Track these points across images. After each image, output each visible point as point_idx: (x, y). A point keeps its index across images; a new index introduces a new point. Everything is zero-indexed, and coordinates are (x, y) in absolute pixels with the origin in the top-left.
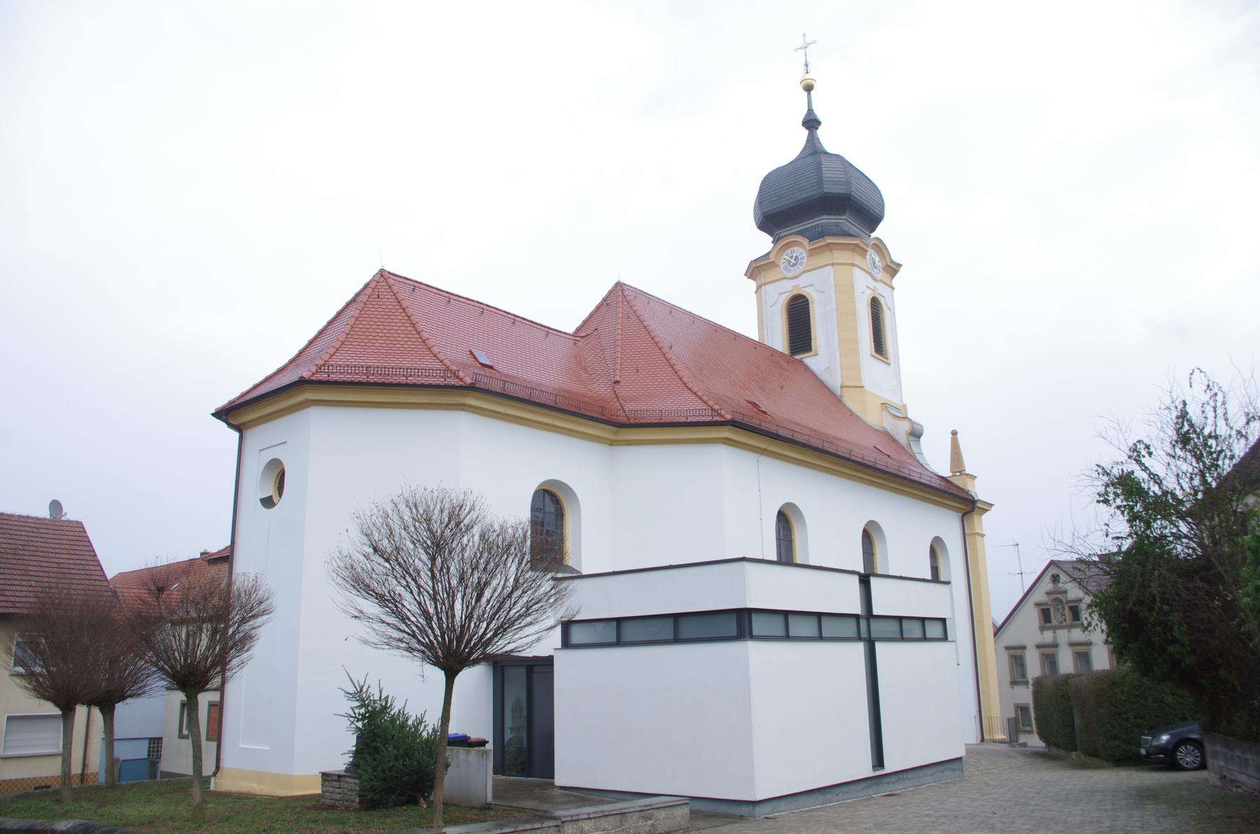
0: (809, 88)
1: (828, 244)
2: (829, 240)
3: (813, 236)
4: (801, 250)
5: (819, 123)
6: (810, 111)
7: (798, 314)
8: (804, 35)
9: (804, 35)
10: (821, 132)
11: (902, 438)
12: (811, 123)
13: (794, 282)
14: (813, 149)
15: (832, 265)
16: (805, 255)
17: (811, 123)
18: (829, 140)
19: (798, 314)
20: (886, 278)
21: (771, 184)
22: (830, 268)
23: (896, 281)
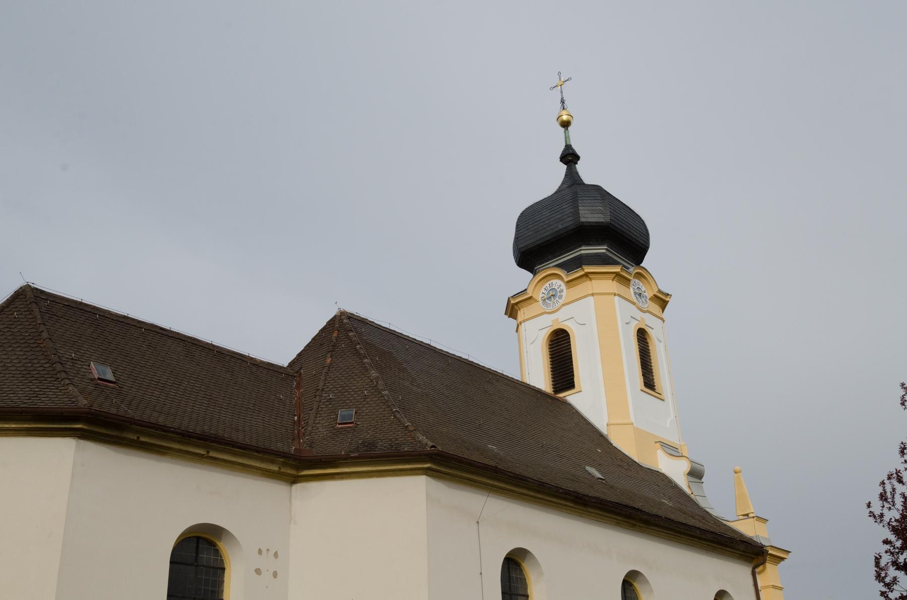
0: (566, 125)
1: (586, 275)
2: (588, 269)
3: (568, 267)
5: (578, 158)
6: (568, 147)
7: (560, 347)
8: (559, 74)
9: (559, 74)
10: (580, 167)
11: (682, 481)
12: (570, 157)
14: (572, 179)
15: (593, 295)
16: (563, 287)
17: (570, 157)
18: (587, 173)
19: (560, 347)
20: (655, 308)
21: (528, 219)
22: (591, 298)
23: (667, 313)
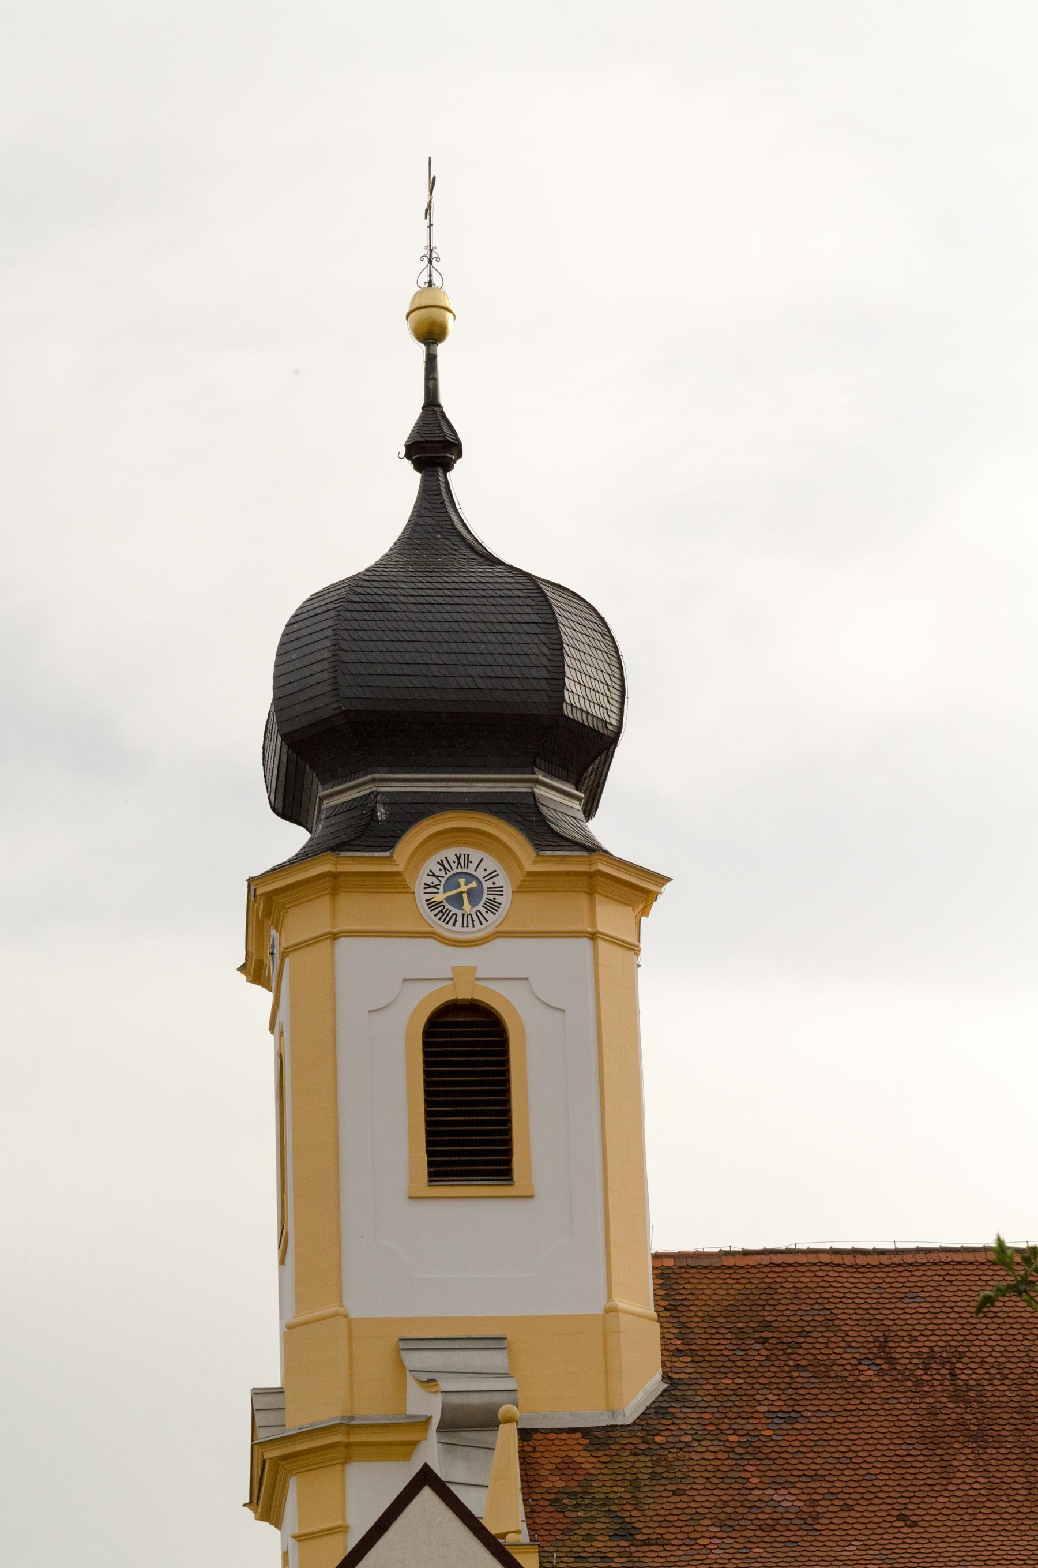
0: (431, 335)
4: (490, 863)
12: (433, 448)
13: (464, 957)
15: (593, 936)
17: (433, 448)
22: (586, 942)
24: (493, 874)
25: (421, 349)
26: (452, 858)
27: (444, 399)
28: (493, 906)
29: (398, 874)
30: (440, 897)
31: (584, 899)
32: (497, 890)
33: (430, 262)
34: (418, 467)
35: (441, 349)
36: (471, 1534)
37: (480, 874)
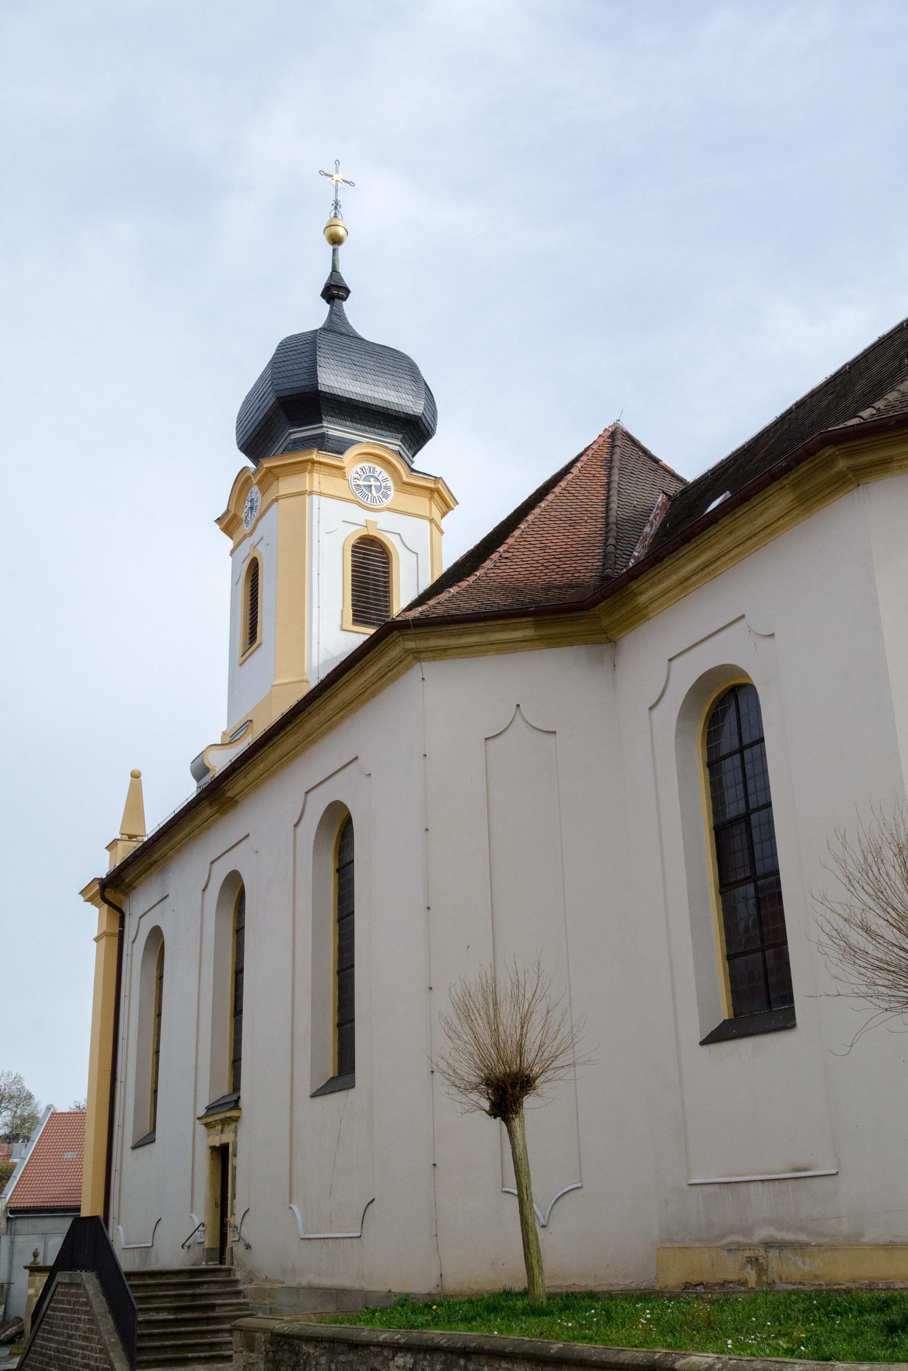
0: (336, 241)
4: (385, 475)
12: (335, 292)
17: (335, 292)
24: (386, 480)
25: (330, 248)
26: (367, 468)
27: (341, 269)
28: (386, 496)
29: (341, 468)
30: (361, 483)
31: (426, 500)
32: (388, 488)
33: (336, 208)
34: (328, 302)
35: (341, 249)
36: (342, 659)
37: (380, 478)
